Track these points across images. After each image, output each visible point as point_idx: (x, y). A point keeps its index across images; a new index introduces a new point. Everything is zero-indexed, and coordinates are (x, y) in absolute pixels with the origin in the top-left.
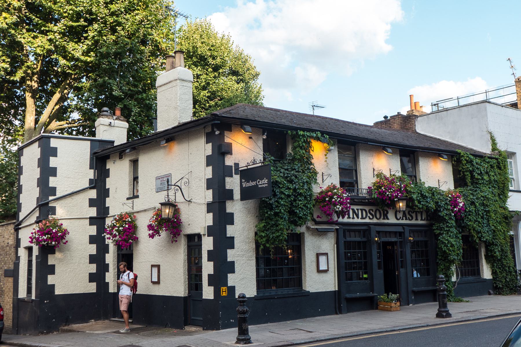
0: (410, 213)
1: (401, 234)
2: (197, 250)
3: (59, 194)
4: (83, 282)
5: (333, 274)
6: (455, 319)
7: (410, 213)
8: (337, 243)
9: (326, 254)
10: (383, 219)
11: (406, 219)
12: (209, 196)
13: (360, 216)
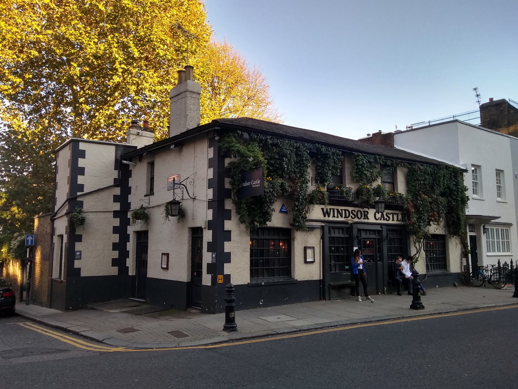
0: (388, 214)
1: (379, 232)
2: (199, 241)
3: (86, 190)
4: (106, 266)
5: (318, 265)
6: (428, 311)
7: (388, 214)
8: (323, 238)
9: (313, 248)
10: (363, 219)
11: (384, 219)
12: (210, 194)
13: (344, 216)
